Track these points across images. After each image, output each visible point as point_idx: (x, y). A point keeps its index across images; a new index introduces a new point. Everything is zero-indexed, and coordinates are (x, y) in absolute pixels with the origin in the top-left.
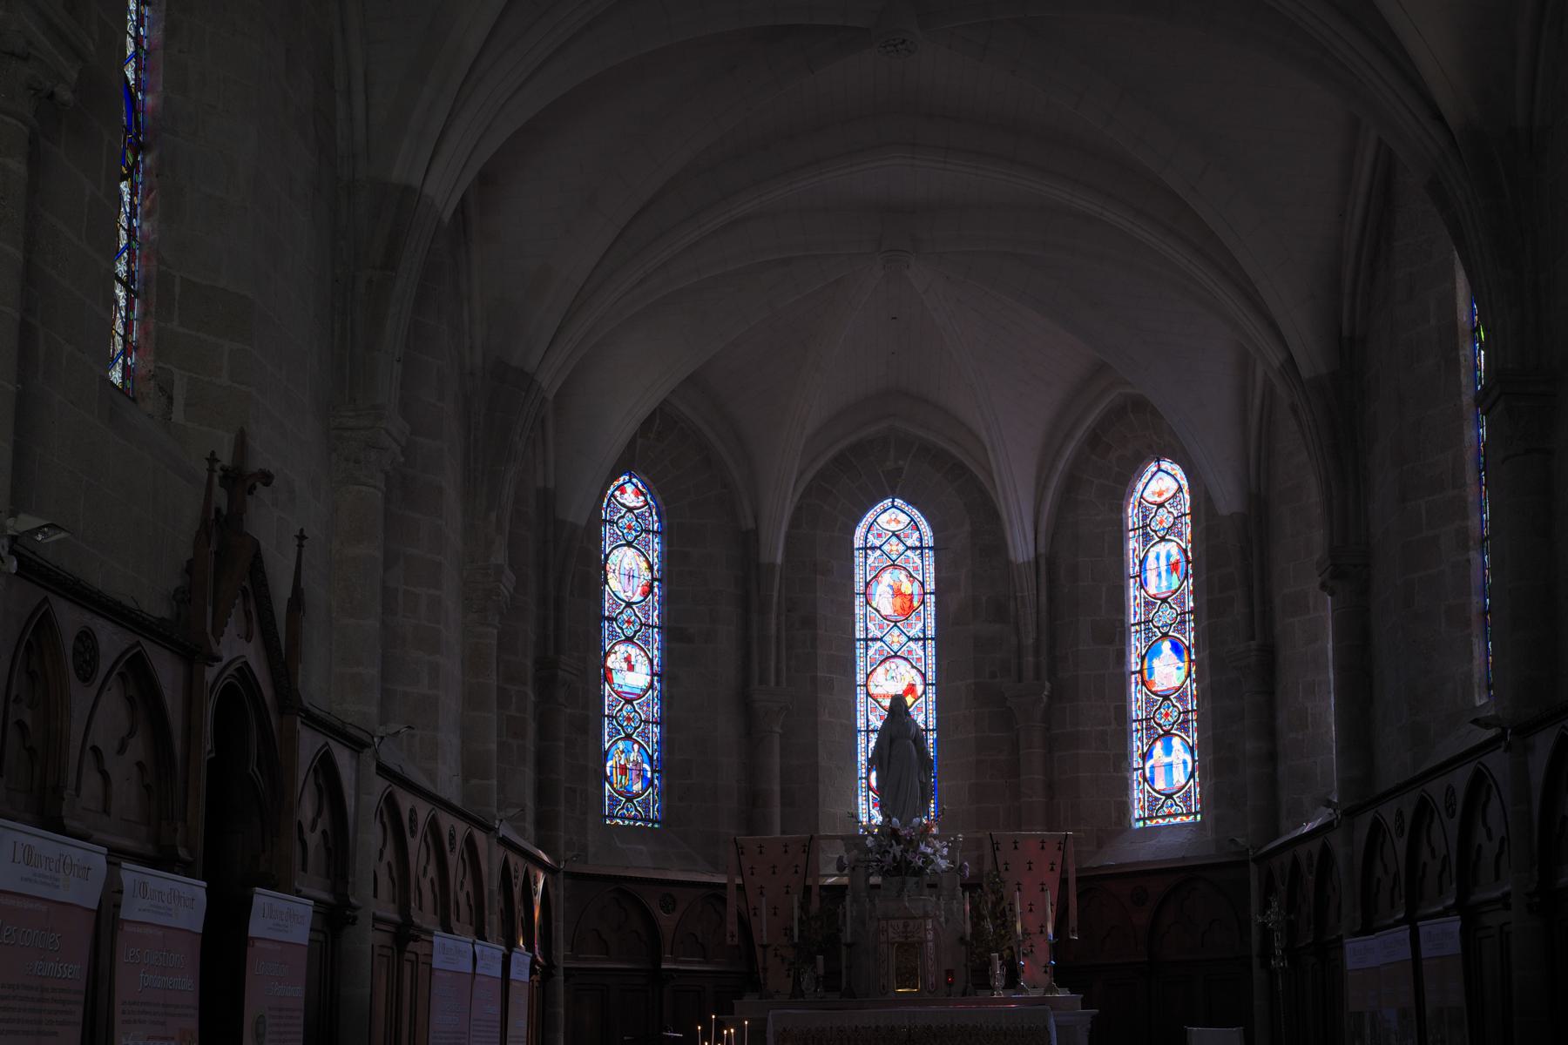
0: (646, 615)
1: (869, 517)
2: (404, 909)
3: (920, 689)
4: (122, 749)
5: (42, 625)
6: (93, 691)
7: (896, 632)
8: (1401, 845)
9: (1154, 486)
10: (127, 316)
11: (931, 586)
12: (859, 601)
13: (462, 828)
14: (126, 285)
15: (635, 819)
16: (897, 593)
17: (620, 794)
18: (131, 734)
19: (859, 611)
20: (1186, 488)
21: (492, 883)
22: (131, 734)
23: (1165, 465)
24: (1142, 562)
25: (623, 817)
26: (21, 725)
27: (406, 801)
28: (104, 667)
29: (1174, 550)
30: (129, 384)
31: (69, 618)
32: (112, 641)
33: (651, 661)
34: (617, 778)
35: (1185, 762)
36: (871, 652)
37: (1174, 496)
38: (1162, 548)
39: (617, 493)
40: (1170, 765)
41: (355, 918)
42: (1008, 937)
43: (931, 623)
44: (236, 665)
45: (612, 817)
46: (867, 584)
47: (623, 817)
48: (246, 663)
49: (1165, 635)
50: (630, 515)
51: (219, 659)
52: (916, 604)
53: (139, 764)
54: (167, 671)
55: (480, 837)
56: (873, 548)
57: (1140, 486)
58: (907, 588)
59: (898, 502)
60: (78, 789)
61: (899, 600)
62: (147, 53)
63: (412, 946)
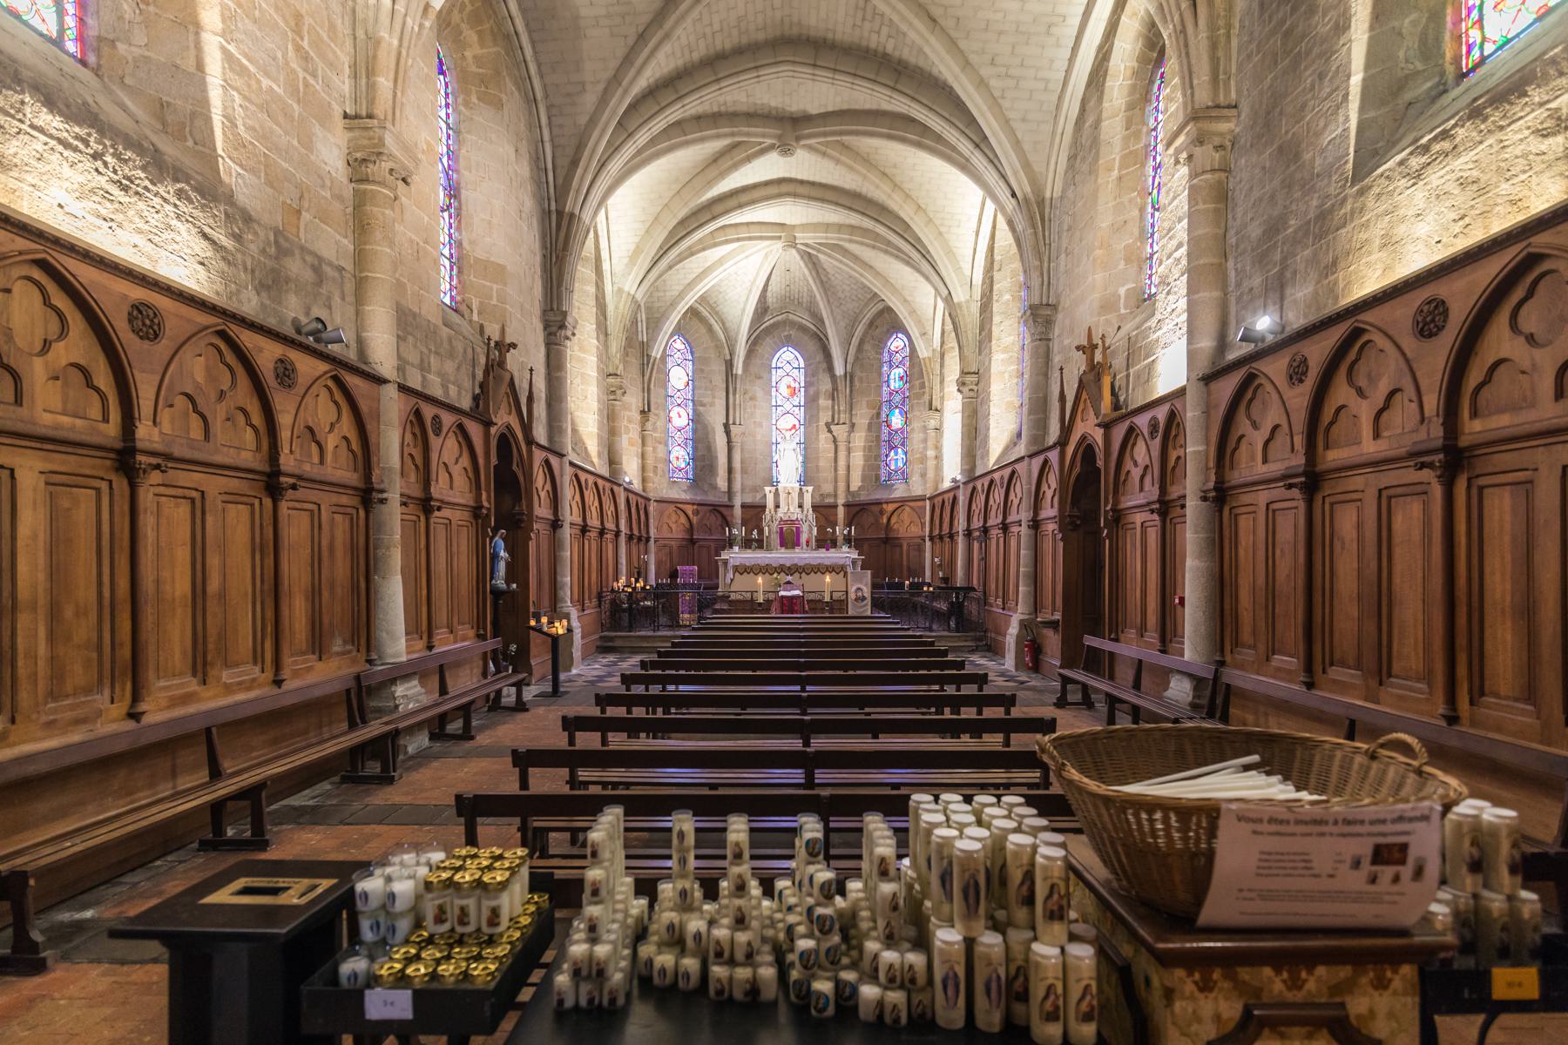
2: (602, 523)
4: (457, 462)
8: (983, 498)
9: (895, 344)
11: (803, 384)
13: (608, 485)
16: (789, 387)
18: (461, 455)
19: (774, 393)
22: (461, 455)
23: (900, 335)
26: (410, 455)
27: (583, 476)
28: (445, 430)
32: (448, 419)
42: (1278, 110)
54: (474, 429)
55: (616, 488)
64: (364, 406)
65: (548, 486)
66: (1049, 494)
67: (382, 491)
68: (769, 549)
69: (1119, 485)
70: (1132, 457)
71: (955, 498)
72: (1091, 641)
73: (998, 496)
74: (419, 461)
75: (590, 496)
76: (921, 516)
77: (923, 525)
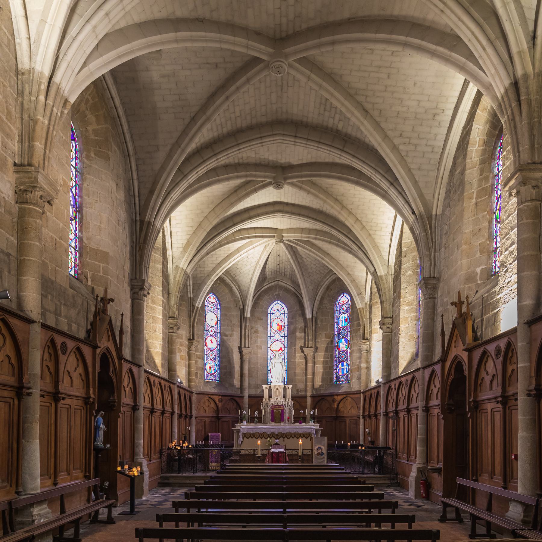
0: (216, 329)
1: (271, 306)
2: (152, 404)
3: (283, 349)
5: (52, 341)
6: (66, 357)
7: (278, 334)
8: (395, 393)
9: (342, 300)
10: (75, 257)
11: (286, 323)
12: (269, 326)
13: (167, 384)
14: (74, 249)
15: (213, 380)
16: (278, 325)
17: (209, 373)
18: (78, 366)
20: (350, 301)
21: (176, 397)
22: (78, 366)
24: (338, 319)
25: (210, 379)
26: (47, 366)
27: (152, 379)
28: (69, 351)
29: (346, 316)
30: (76, 275)
31: (59, 340)
32: (71, 345)
33: (217, 341)
34: (208, 370)
35: (347, 368)
36: (271, 340)
37: (347, 302)
38: (343, 316)
39: (209, 299)
40: (343, 369)
41: (139, 408)
43: (286, 332)
44: (106, 347)
45: (207, 379)
46: (271, 323)
47: (210, 379)
48: (108, 347)
49: (343, 337)
50: (212, 304)
51: (100, 347)
52: (283, 328)
53: (80, 374)
54: (87, 351)
56: (272, 314)
57: (339, 300)
58: (281, 324)
59: (279, 302)
60: (63, 382)
61: (278, 327)
62: (78, 185)
63: (154, 413)
64: (20, 337)
65: (131, 385)
66: (435, 391)
67: (29, 388)
68: (265, 423)
69: (477, 385)
70: (485, 370)
71: (378, 393)
72: (460, 481)
73: (404, 392)
74: (52, 369)
75: (156, 391)
76: (358, 403)
77: (359, 409)
